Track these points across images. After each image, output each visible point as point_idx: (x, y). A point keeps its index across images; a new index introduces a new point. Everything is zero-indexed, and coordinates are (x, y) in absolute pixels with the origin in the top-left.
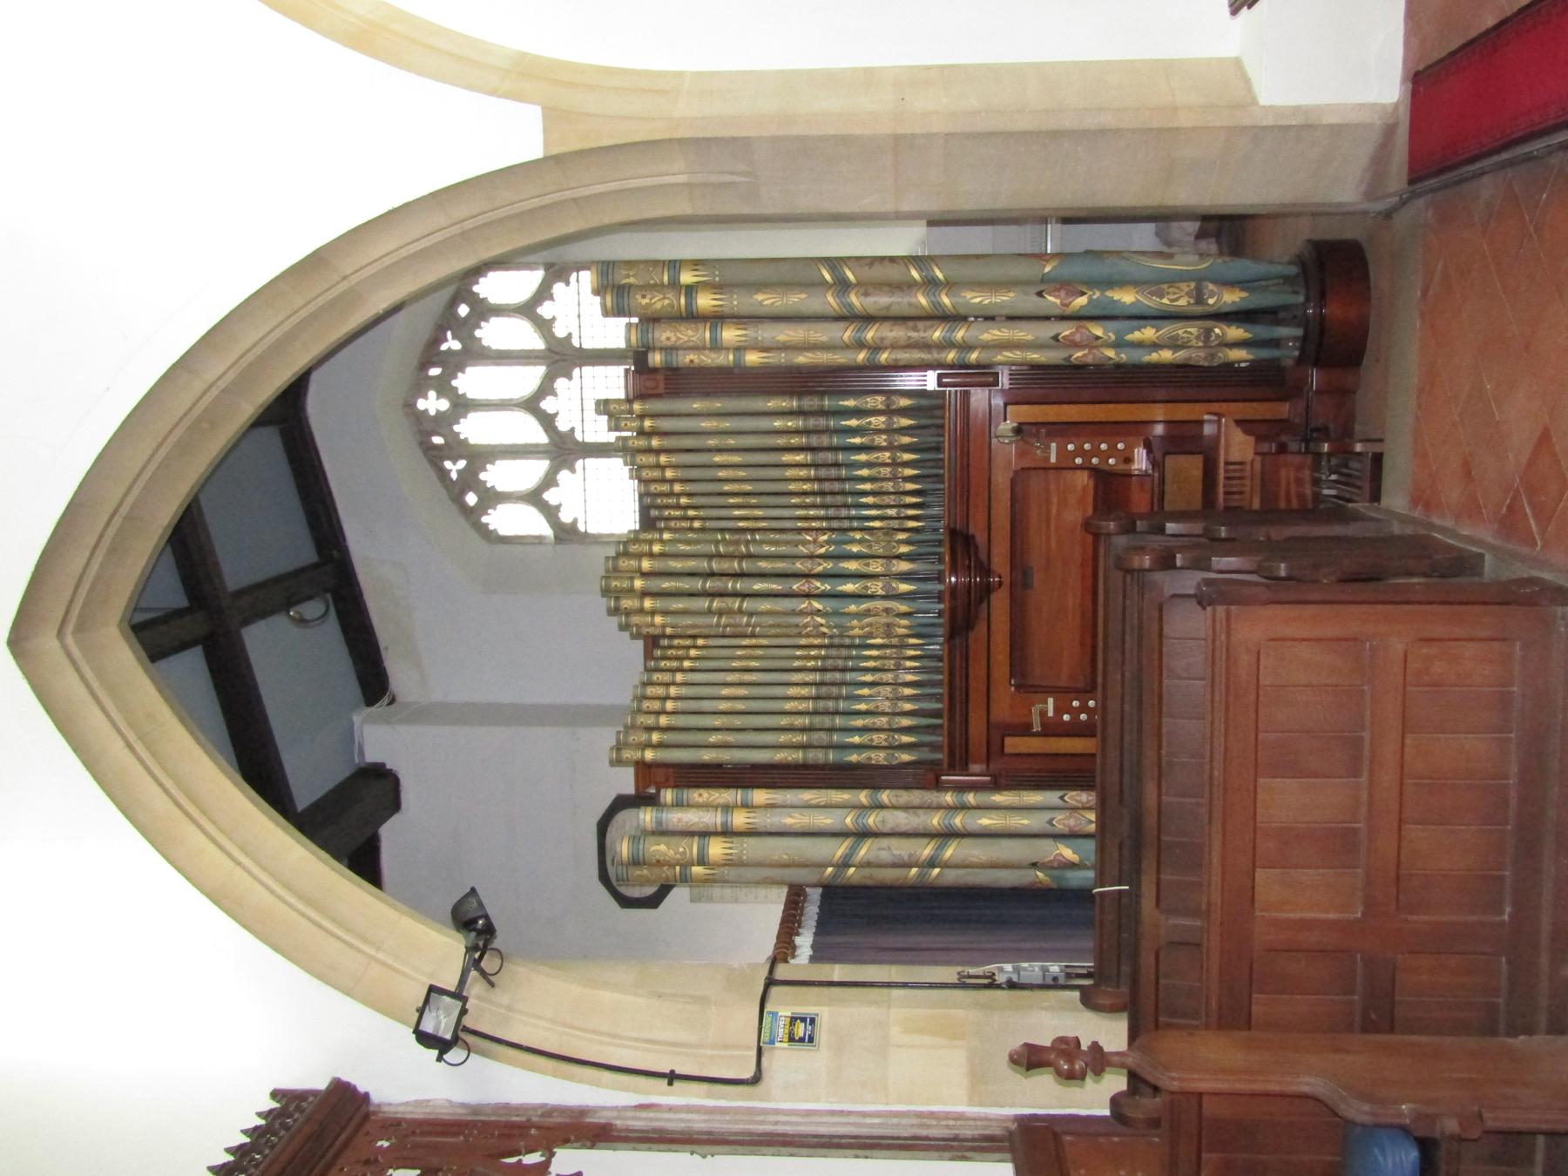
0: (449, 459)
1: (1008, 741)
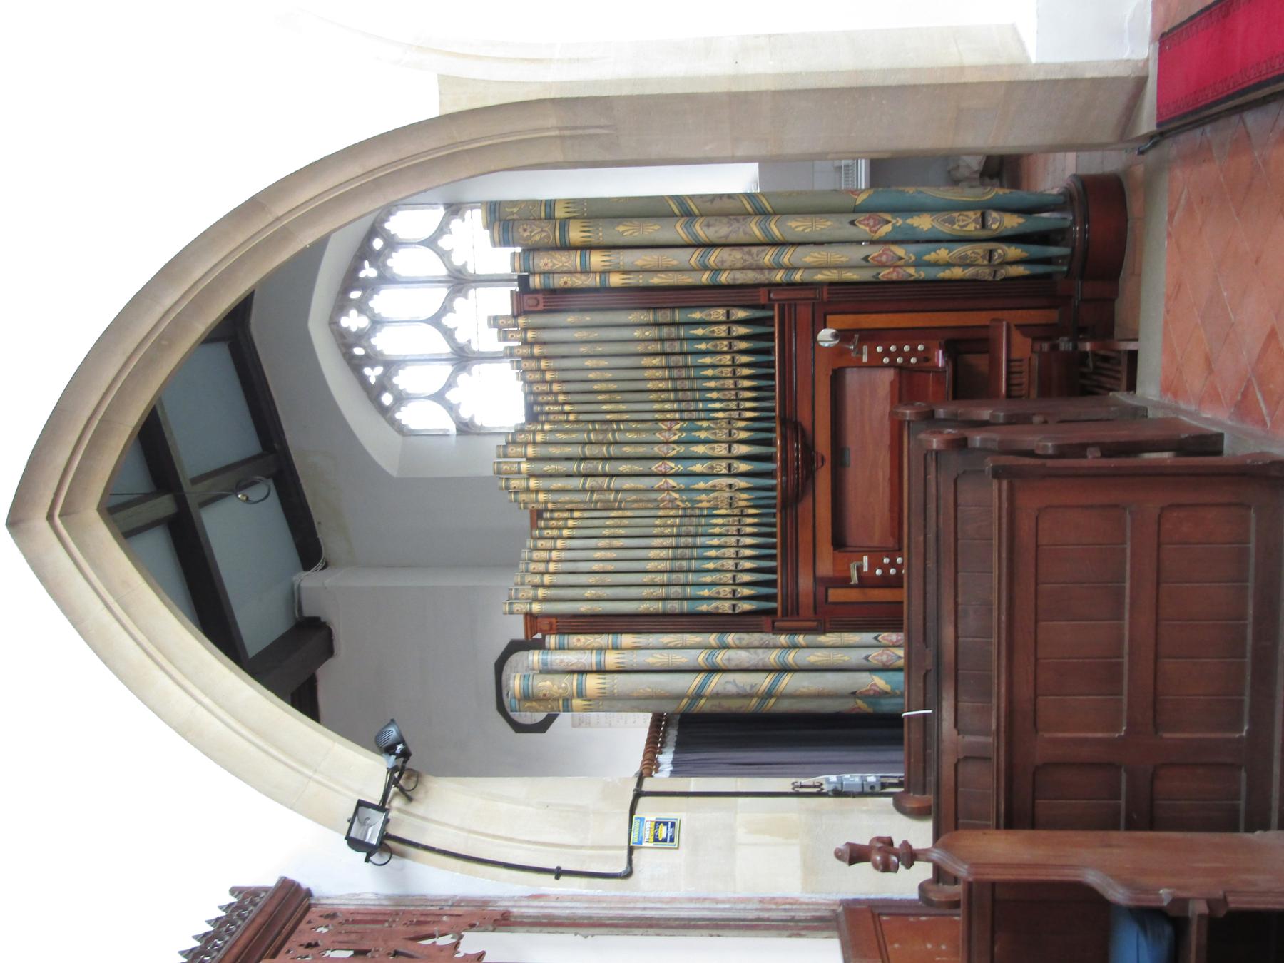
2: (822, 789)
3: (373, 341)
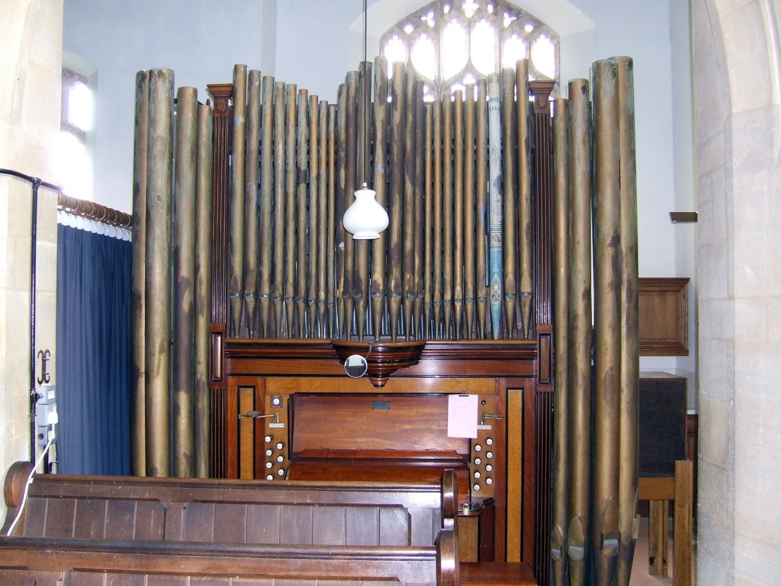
0: (435, 15)
1: (250, 391)
2: (40, 383)
3: (454, 21)
